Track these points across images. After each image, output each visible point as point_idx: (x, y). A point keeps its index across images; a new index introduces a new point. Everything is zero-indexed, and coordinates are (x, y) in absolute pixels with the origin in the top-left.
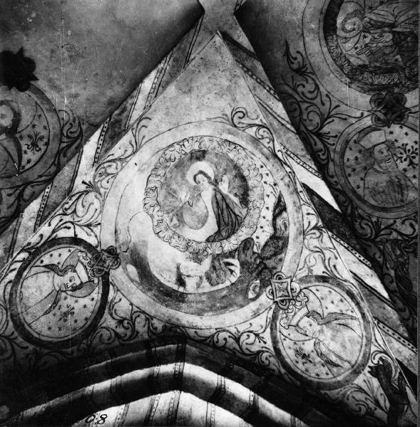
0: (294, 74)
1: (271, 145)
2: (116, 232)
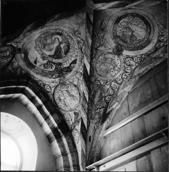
0: (100, 30)
1: (82, 46)
2: (24, 44)
